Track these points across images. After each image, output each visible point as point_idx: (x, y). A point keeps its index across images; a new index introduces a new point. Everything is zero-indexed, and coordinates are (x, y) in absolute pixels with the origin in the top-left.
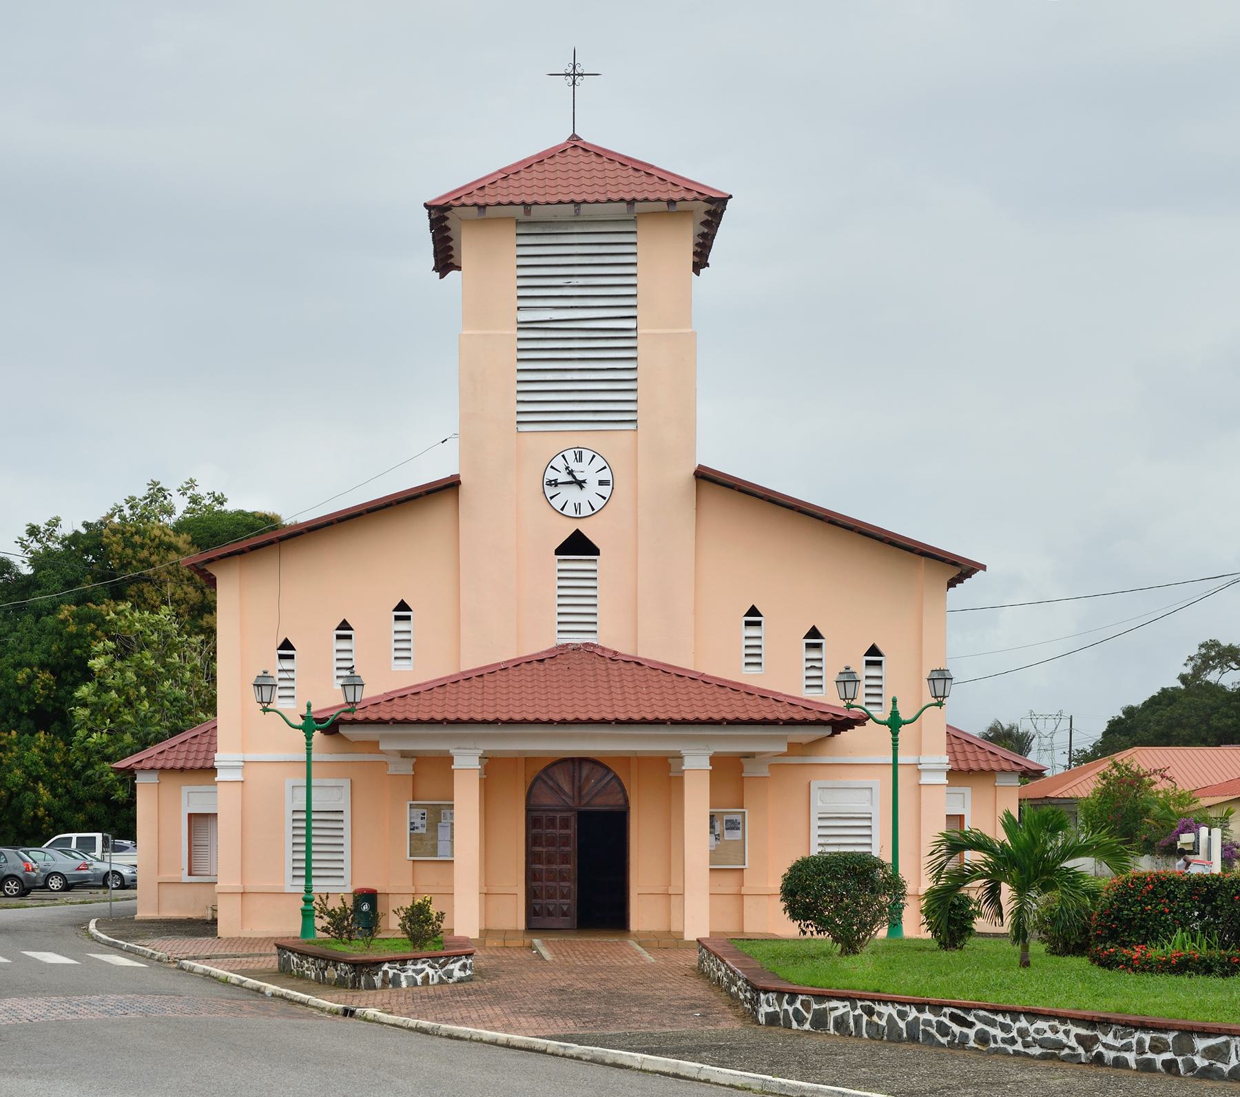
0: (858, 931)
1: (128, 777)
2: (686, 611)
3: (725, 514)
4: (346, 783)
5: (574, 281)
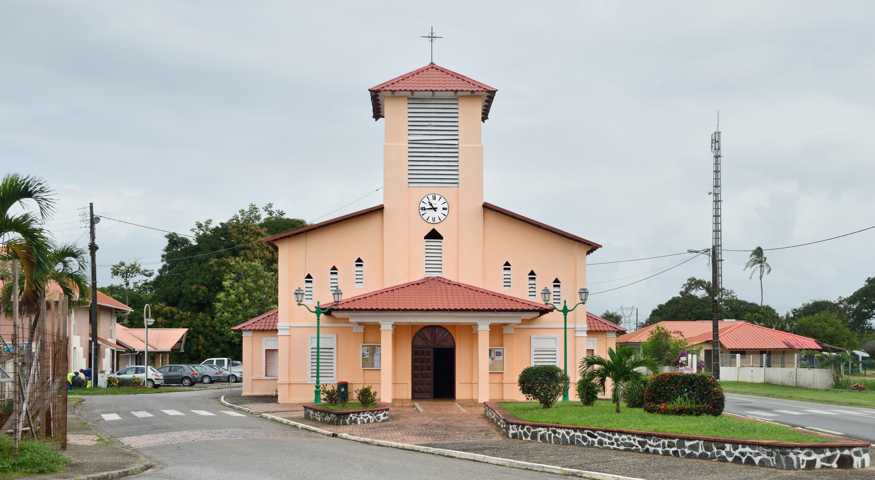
2: (476, 263)
5: (432, 124)
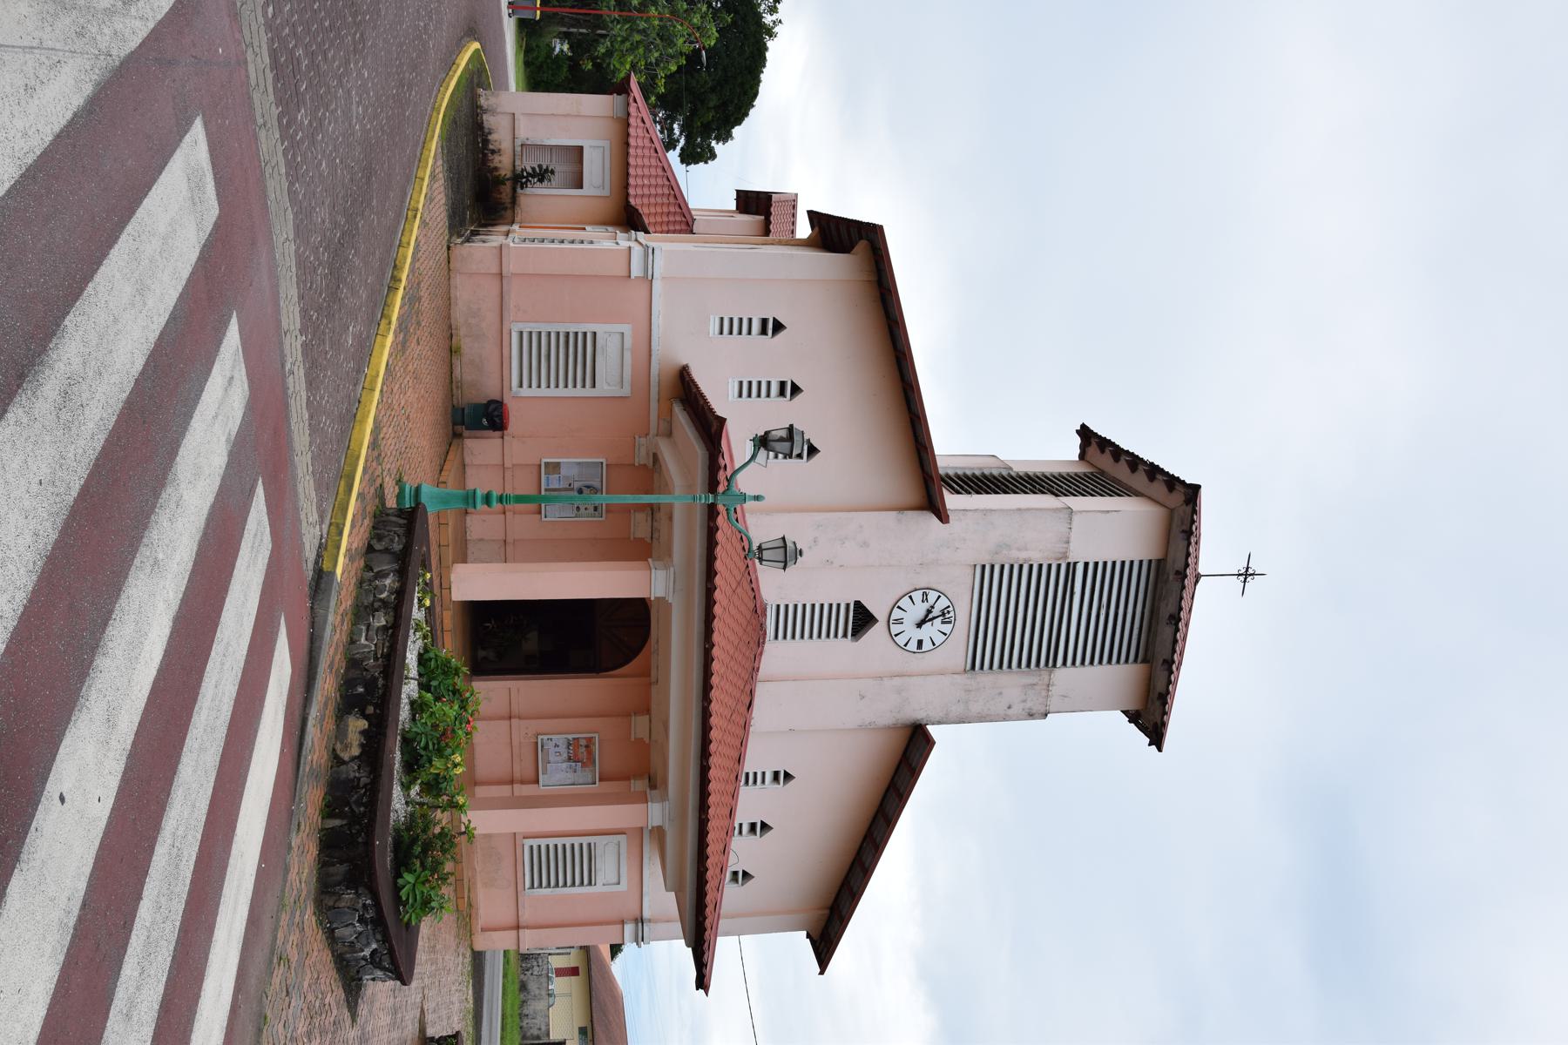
0: (294, 156)
1: (622, 89)
2: (801, 717)
3: (896, 743)
4: (626, 391)
5: (1103, 612)
